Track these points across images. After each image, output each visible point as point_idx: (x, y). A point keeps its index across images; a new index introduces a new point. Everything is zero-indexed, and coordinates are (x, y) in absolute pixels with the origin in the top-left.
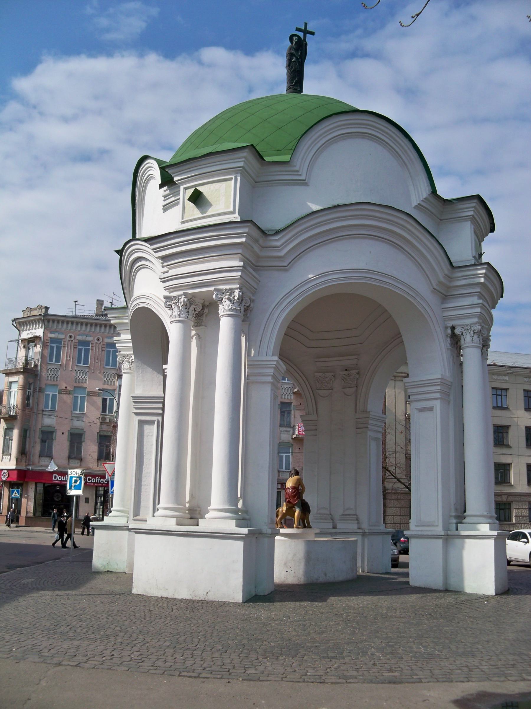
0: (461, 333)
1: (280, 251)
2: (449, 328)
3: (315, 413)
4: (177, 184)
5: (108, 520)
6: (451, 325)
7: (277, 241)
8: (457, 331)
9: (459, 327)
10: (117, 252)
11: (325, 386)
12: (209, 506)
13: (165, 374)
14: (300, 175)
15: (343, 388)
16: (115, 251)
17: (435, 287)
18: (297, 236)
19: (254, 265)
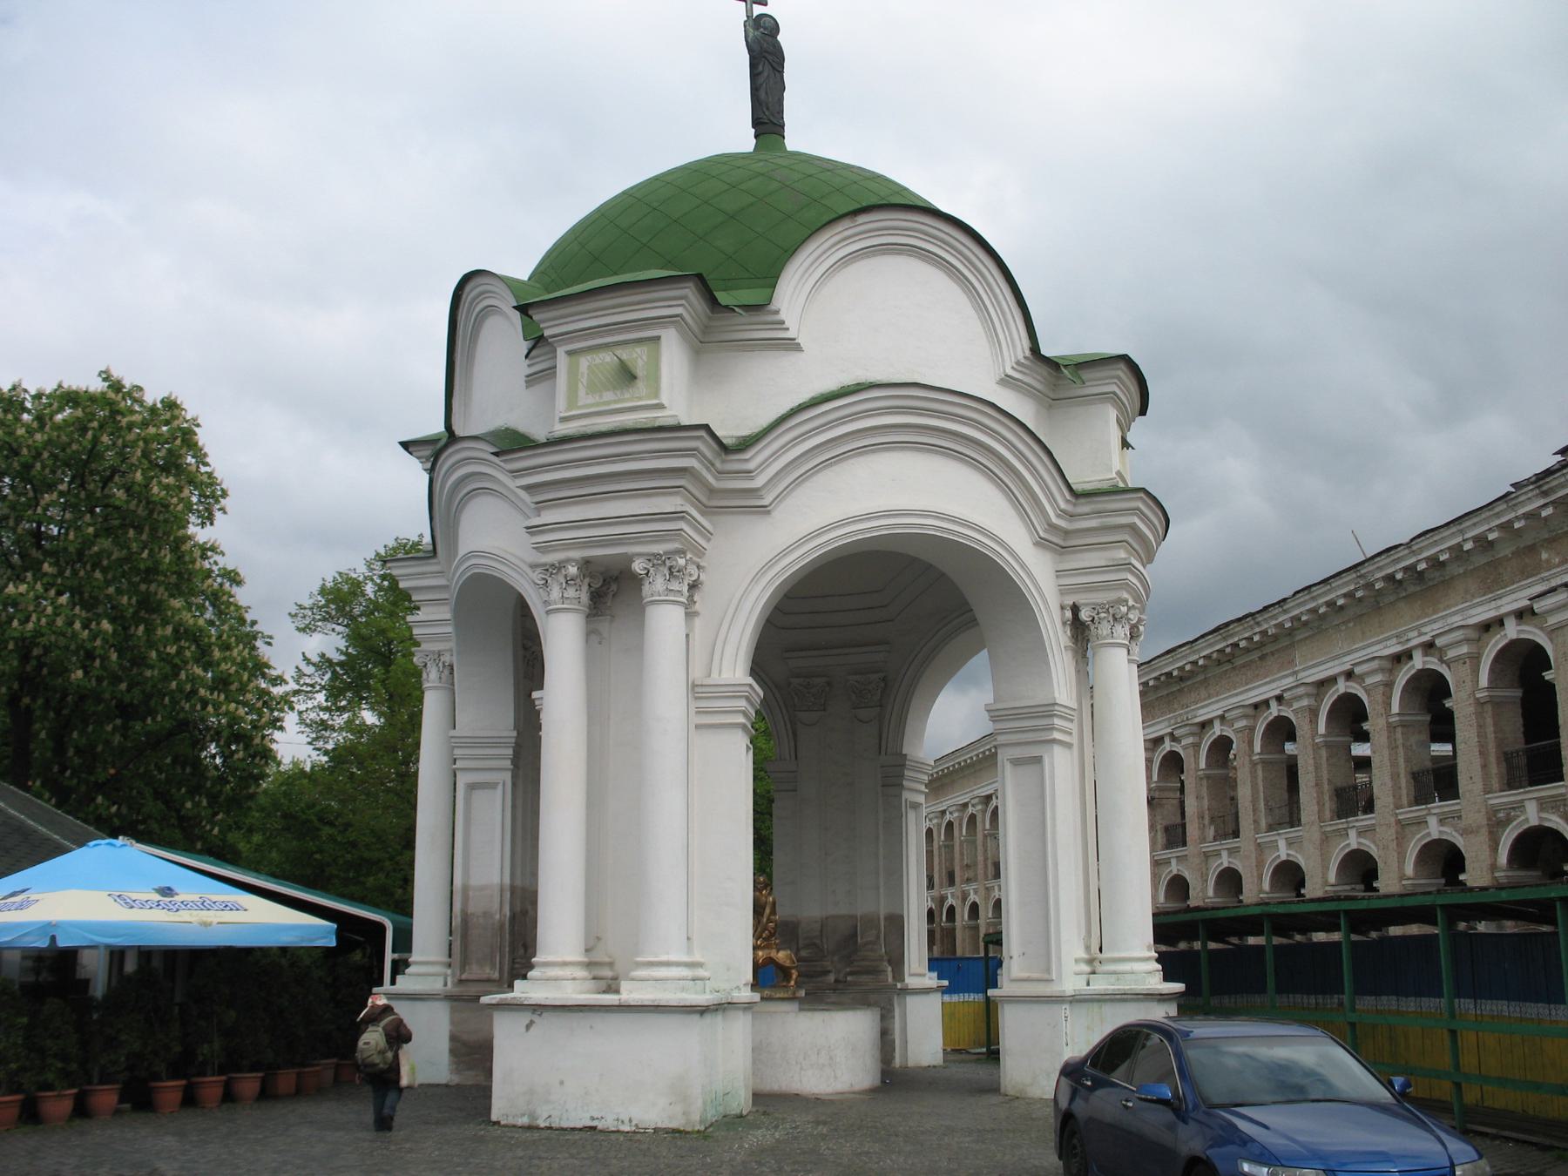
0: (1091, 619)
1: (752, 478)
2: (1069, 608)
4: (549, 344)
5: (523, 991)
6: (1071, 603)
7: (754, 458)
8: (1084, 615)
9: (1089, 608)
12: (534, 957)
13: (537, 708)
14: (788, 329)
17: (1042, 534)
19: (704, 505)
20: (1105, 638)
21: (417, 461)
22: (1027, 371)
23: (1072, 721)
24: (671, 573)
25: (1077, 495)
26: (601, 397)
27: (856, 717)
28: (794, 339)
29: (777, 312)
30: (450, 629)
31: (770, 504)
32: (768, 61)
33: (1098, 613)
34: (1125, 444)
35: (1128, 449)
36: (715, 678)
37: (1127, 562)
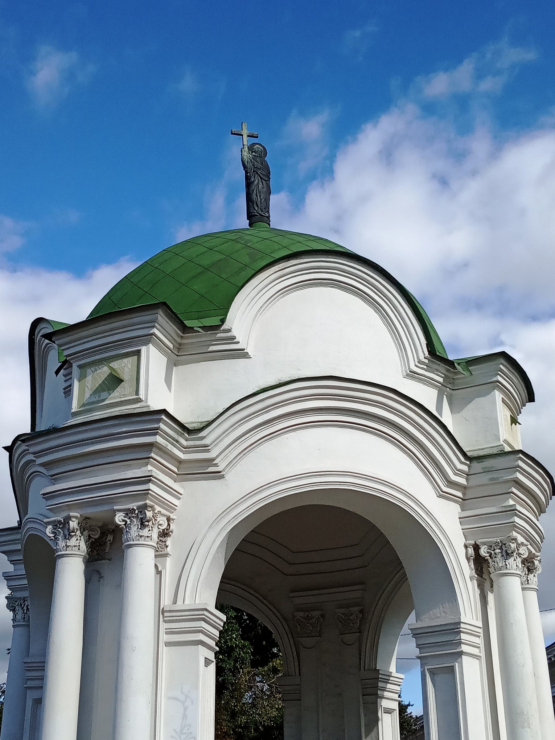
1: (208, 451)
3: (297, 672)
8: (483, 551)
10: (5, 448)
11: (310, 632)
14: (238, 343)
15: (341, 634)
16: (3, 447)
18: (7, 544)
20: (500, 570)
23: (479, 637)
24: (142, 524)
26: (99, 396)
27: (342, 641)
28: (244, 350)
29: (229, 330)
30: (25, 582)
31: (224, 470)
33: (494, 550)
34: (514, 421)
35: (516, 424)
36: (180, 605)
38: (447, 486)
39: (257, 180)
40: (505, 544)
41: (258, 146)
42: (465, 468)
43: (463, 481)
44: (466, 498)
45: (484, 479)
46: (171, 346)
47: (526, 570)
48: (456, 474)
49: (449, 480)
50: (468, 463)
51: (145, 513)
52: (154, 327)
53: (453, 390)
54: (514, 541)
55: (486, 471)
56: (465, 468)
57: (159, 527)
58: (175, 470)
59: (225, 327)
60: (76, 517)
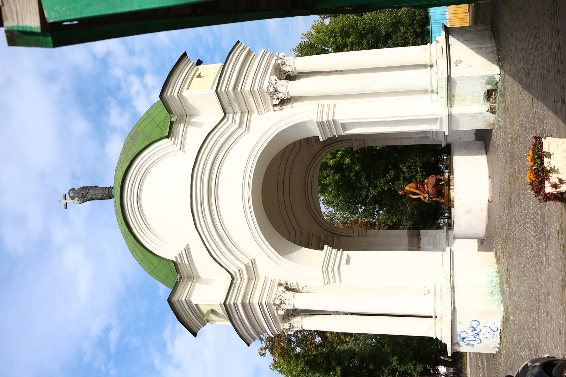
1: (242, 269)
3: (351, 141)
8: (276, 102)
14: (182, 252)
21: (252, 115)
22: (176, 139)
25: (225, 113)
31: (250, 259)
32: (85, 195)
35: (201, 75)
37: (250, 92)
38: (242, 127)
39: (89, 196)
40: (271, 93)
41: (70, 194)
42: (231, 116)
43: (238, 116)
44: (248, 111)
45: (236, 105)
46: (190, 283)
47: (284, 66)
48: (235, 123)
49: (239, 127)
50: (227, 115)
51: (279, 63)
52: (181, 300)
53: (187, 115)
54: (268, 89)
55: (231, 104)
56: (231, 116)
57: (284, 56)
58: (254, 281)
59: (174, 260)
60: (283, 326)
